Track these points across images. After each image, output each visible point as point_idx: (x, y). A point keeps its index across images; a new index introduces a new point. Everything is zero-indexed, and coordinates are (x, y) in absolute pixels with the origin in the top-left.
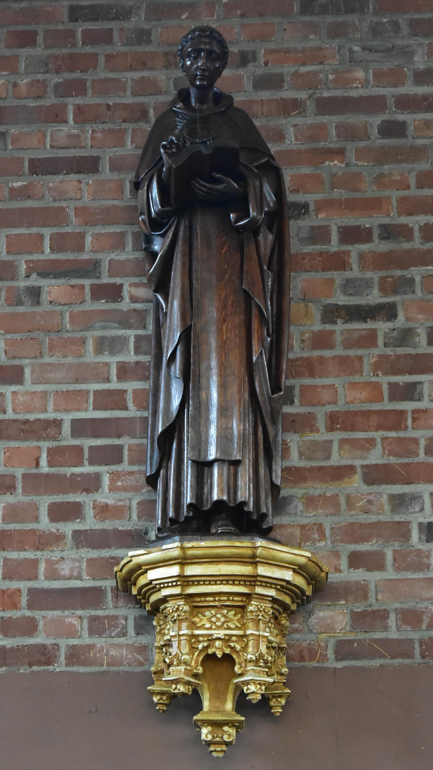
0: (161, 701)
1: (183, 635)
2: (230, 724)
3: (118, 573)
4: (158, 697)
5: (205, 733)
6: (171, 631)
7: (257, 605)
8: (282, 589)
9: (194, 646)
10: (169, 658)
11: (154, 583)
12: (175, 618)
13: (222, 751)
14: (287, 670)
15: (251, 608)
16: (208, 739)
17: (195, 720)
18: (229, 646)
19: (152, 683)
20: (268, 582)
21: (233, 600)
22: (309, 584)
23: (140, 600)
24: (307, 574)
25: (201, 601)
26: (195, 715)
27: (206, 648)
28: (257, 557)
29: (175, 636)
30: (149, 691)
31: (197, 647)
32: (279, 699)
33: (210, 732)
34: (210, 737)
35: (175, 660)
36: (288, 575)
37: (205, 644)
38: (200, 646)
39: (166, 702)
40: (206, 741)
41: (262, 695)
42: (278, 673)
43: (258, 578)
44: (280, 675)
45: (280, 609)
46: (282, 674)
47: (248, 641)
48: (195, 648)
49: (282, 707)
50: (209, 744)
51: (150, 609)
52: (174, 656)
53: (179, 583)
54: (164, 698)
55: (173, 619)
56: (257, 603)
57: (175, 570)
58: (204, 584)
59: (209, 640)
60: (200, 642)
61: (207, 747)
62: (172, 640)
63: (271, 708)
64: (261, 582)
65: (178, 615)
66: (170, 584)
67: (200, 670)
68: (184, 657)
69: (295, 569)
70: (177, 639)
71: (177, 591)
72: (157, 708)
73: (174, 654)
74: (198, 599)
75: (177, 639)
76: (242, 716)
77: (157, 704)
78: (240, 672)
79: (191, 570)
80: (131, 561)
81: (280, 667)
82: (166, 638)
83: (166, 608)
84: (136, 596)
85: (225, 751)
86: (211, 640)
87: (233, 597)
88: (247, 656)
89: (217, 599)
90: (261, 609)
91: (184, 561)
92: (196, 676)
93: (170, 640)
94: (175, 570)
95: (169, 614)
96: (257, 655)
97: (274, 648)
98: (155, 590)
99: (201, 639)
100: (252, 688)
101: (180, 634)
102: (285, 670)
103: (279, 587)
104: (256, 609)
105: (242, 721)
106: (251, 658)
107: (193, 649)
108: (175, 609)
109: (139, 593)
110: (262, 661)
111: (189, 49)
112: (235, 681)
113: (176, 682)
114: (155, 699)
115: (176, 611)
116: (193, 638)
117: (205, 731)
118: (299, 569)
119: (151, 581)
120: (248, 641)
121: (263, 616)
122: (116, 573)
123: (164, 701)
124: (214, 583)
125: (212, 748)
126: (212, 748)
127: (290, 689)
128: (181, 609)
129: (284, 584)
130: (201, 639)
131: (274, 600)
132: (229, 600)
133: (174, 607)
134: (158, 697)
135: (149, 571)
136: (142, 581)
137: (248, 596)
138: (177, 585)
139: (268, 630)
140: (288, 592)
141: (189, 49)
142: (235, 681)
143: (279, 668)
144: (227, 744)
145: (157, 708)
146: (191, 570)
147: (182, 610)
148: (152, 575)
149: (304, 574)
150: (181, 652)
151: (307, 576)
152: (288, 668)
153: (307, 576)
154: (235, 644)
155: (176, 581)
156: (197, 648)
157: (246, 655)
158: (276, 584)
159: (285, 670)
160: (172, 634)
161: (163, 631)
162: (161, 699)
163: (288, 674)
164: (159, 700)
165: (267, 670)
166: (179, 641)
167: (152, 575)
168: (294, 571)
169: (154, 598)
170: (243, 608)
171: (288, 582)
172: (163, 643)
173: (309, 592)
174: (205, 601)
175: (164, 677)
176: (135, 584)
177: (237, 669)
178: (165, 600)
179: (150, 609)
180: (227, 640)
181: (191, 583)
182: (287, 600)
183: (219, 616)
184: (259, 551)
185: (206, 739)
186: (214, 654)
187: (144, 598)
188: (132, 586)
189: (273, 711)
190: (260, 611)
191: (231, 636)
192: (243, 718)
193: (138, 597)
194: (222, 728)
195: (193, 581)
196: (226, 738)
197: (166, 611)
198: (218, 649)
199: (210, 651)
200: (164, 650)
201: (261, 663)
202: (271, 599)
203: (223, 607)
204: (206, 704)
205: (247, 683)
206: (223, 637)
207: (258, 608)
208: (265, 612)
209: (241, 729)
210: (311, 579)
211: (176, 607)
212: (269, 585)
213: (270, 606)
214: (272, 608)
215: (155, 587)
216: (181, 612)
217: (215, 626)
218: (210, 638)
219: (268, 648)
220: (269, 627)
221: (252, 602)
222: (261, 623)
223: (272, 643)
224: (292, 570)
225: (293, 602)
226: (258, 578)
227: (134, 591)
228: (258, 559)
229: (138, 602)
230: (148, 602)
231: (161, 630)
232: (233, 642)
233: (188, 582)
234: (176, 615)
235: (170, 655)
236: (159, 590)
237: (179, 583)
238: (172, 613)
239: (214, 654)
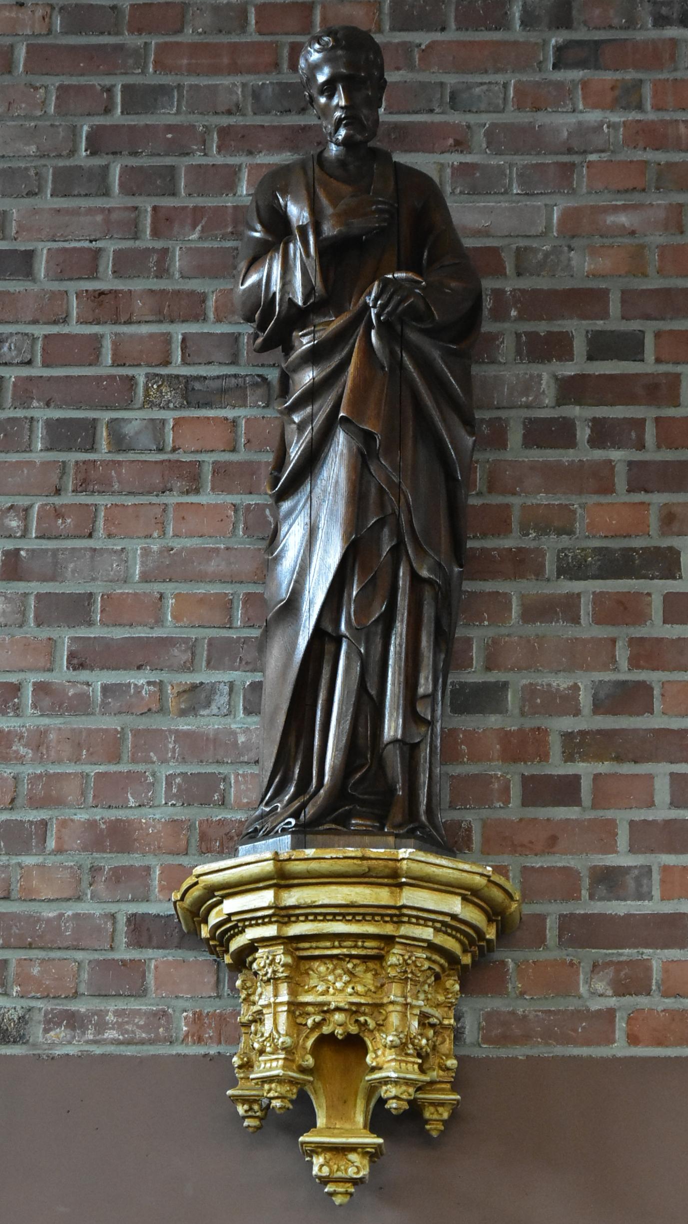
0: (250, 1113)
1: (281, 1004)
2: (360, 1150)
3: (178, 903)
4: (246, 1107)
5: (319, 1165)
6: (265, 996)
7: (402, 955)
8: (443, 929)
9: (299, 1020)
10: (258, 1042)
11: (233, 918)
12: (269, 975)
13: (346, 1193)
14: (455, 1062)
15: (393, 960)
16: (324, 1175)
17: (303, 1143)
18: (357, 1021)
19: (234, 1084)
20: (422, 917)
21: (363, 947)
22: (490, 920)
23: (215, 946)
24: (491, 908)
25: (311, 948)
26: (302, 1135)
27: (317, 1025)
28: (400, 877)
29: (268, 1006)
30: (230, 1097)
31: (304, 1023)
32: (441, 1109)
33: (327, 1163)
34: (326, 1171)
35: (268, 1045)
36: (455, 905)
37: (318, 1018)
38: (310, 1022)
39: (258, 1114)
40: (320, 1178)
41: (409, 1102)
42: (440, 1068)
43: (405, 911)
44: (444, 1071)
45: (442, 961)
46: (448, 1069)
47: (387, 1013)
48: (301, 1024)
49: (445, 1122)
50: (325, 1181)
51: (230, 961)
52: (267, 1038)
53: (273, 919)
54: (256, 1107)
55: (265, 978)
56: (401, 952)
57: (265, 898)
58: (306, 920)
59: (324, 1012)
60: (308, 1014)
61: (322, 1186)
62: (265, 1011)
63: (427, 1122)
64: (410, 916)
65: (274, 972)
66: (260, 921)
67: (310, 1061)
68: (281, 1040)
69: (467, 895)
70: (271, 1010)
71: (270, 931)
72: (246, 1124)
73: (266, 1035)
74: (307, 945)
75: (271, 1010)
76: (379, 1136)
77: (244, 1118)
78: (374, 1064)
79: (292, 897)
80: (196, 883)
81: (444, 1058)
82: (255, 1008)
83: (255, 959)
84: (208, 940)
85: (351, 1194)
86: (325, 1010)
87: (363, 942)
88: (386, 1039)
89: (337, 943)
90: (409, 962)
91: (283, 882)
92: (303, 1070)
93: (260, 1012)
94: (404, 930)
95: (259, 970)
96: (401, 1036)
97: (432, 1026)
98: (236, 930)
99: (310, 1009)
100: (393, 1091)
101: (278, 1001)
102: (452, 1063)
103: (438, 925)
104: (401, 961)
105: (380, 1145)
106: (391, 1041)
107: (296, 1025)
108: (268, 961)
109: (213, 937)
110: (410, 1046)
111: (417, 291)
112: (368, 1078)
113: (270, 1080)
114: (241, 1110)
115: (270, 965)
116: (295, 1008)
117: (318, 1161)
118: (470, 895)
119: (230, 915)
120: (387, 1013)
121: (412, 973)
122: (175, 903)
123: (255, 1112)
124: (340, 918)
125: (328, 1189)
126: (328, 1189)
127: (459, 1094)
128: (277, 961)
129: (448, 919)
130: (310, 1009)
131: (431, 946)
132: (356, 947)
133: (268, 958)
134: (246, 1107)
135: (225, 902)
136: (214, 918)
137: (389, 940)
138: (270, 922)
139: (422, 996)
140: (458, 935)
141: (417, 291)
142: (368, 1078)
143: (442, 1059)
144: (355, 1182)
145: (246, 1124)
146: (292, 897)
147: (279, 963)
148: (231, 905)
149: (482, 904)
150: (278, 1032)
151: (488, 909)
152: (456, 1057)
153: (488, 909)
154: (367, 1018)
155: (269, 916)
156: (306, 1025)
157: (384, 1036)
158: (434, 921)
159: (452, 1063)
160: (262, 1002)
161: (252, 998)
162: (251, 1109)
163: (457, 1068)
164: (246, 1111)
165: (420, 1061)
166: (275, 1014)
167: (231, 905)
168: (465, 899)
169: (236, 944)
170: (379, 958)
171: (454, 917)
172: (250, 1018)
173: (491, 934)
174: (317, 948)
175: (252, 1072)
176: (206, 922)
177: (369, 1059)
178: (252, 947)
179: (230, 961)
180: (353, 1010)
181: (293, 919)
182: (451, 944)
183: (339, 971)
184: (404, 865)
185: (319, 1174)
186: (332, 1034)
187: (221, 945)
188: (202, 925)
189: (428, 1127)
190: (408, 964)
191: (359, 1005)
192: (381, 1141)
193: (211, 943)
194: (346, 1155)
195: (298, 916)
196: (351, 1172)
197: (255, 966)
198: (338, 1026)
199: (326, 1030)
200: (253, 1028)
201: (409, 1049)
202: (425, 945)
203: (347, 959)
204: (321, 1121)
205: (386, 1081)
206: (347, 1007)
207: (405, 960)
208: (417, 966)
209: (378, 1158)
210: (495, 913)
211: (271, 958)
212: (422, 922)
213: (425, 956)
214: (428, 959)
215: (236, 926)
216: (277, 965)
217: (333, 989)
218: (325, 1008)
219: (422, 1024)
220: (425, 992)
221: (395, 951)
222: (409, 983)
223: (428, 1018)
224: (459, 898)
225: (465, 951)
226: (405, 911)
227: (205, 932)
228: (404, 880)
229: (212, 950)
230: (227, 951)
231: (249, 995)
232: (364, 1014)
233: (289, 916)
234: (270, 971)
235: (262, 1036)
236: (242, 931)
237: (273, 919)
238: (264, 967)
239: (332, 1034)
